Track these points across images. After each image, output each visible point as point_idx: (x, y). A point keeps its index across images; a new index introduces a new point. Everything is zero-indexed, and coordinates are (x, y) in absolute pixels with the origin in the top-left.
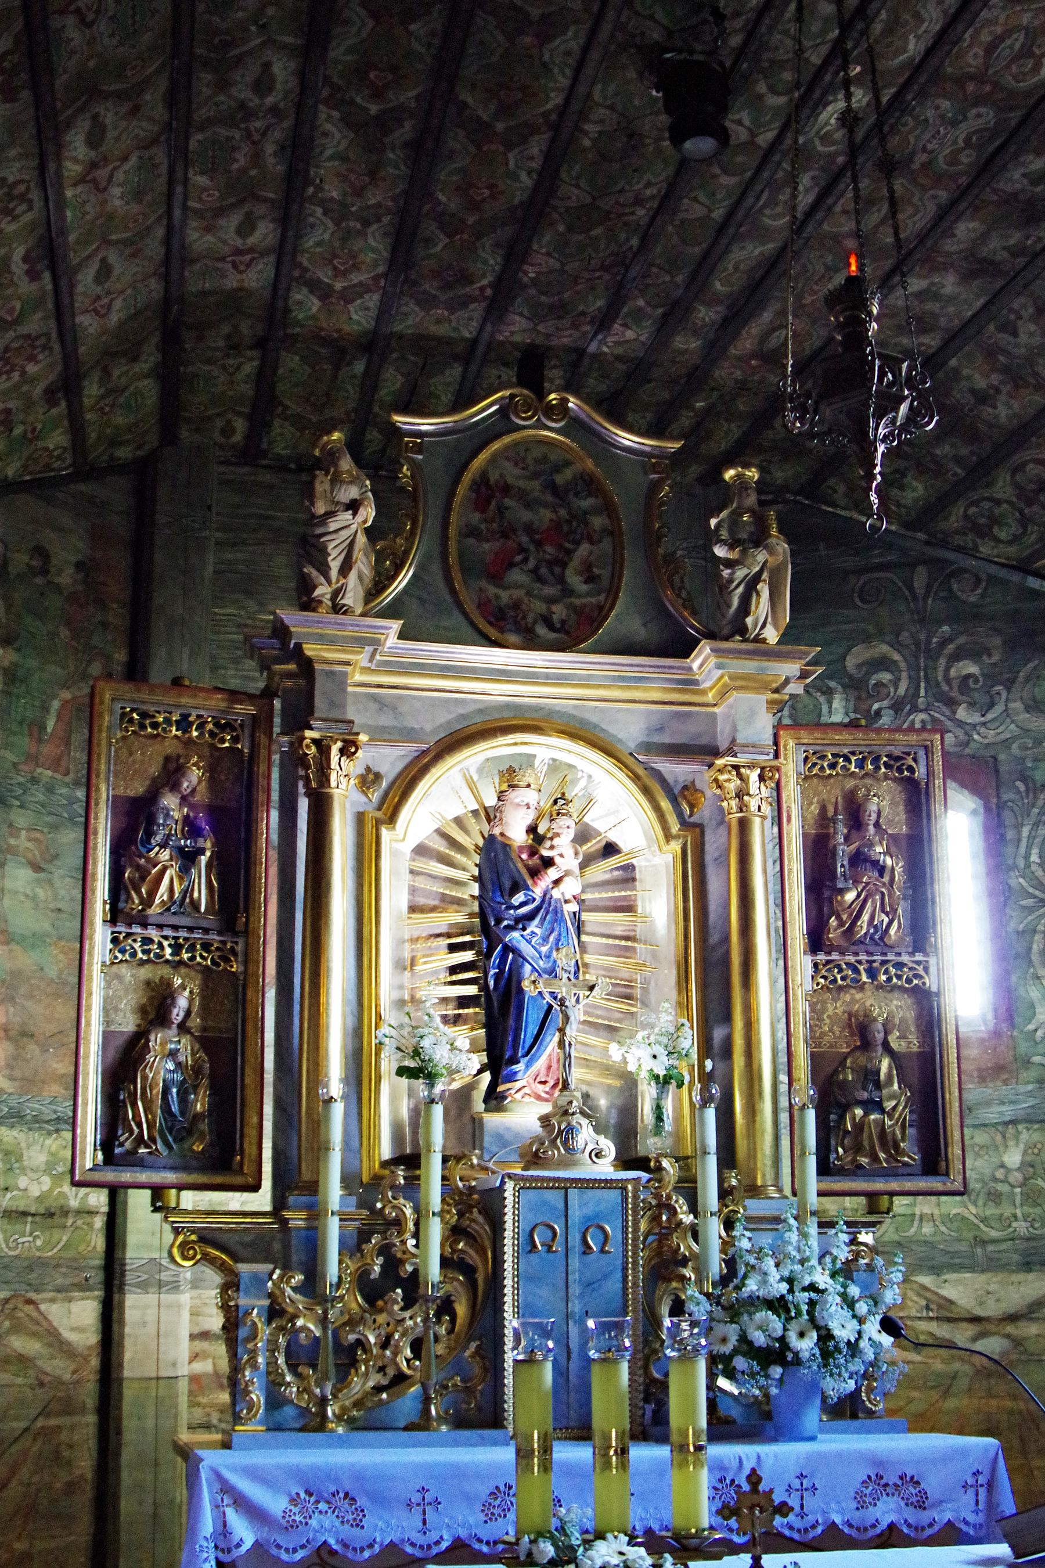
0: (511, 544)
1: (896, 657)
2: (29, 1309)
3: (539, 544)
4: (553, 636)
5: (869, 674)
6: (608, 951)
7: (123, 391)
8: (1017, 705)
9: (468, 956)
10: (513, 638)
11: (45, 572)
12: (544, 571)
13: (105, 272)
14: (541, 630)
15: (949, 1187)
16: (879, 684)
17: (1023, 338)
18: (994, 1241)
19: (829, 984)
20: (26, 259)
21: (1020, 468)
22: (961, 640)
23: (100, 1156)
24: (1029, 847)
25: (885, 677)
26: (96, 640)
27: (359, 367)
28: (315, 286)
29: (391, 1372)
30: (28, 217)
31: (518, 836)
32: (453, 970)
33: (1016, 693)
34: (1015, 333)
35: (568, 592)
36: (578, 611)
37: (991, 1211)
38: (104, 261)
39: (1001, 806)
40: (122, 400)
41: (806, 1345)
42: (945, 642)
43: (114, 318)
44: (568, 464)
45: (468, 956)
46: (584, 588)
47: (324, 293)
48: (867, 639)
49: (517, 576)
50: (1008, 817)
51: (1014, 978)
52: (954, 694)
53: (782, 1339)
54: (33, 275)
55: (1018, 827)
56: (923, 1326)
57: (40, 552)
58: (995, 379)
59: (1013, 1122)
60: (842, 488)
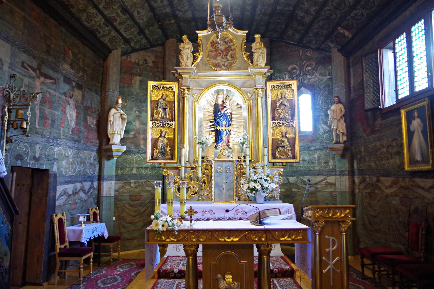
0: (218, 52)
1: (297, 67)
2: (149, 183)
3: (222, 52)
4: (225, 68)
5: (292, 70)
6: (237, 122)
7: (154, 32)
8: (318, 74)
9: (213, 123)
10: (218, 69)
11: (146, 63)
12: (223, 57)
13: (139, 13)
14: (223, 67)
15: (296, 161)
16: (294, 72)
17: (306, 5)
18: (313, 171)
19: (276, 126)
20: (121, 12)
21: (312, 30)
22: (308, 63)
23: (151, 158)
24: (319, 100)
25: (295, 71)
26: (157, 74)
27: (194, 23)
28: (179, 10)
29: (195, 192)
30: (118, 5)
31: (220, 102)
32: (211, 126)
33: (318, 72)
34: (304, 5)
35: (228, 60)
36: (230, 63)
37: (312, 165)
38: (137, 11)
39: (315, 93)
40: (154, 33)
41: (259, 188)
42: (305, 64)
43: (145, 20)
44: (227, 37)
45: (213, 123)
46: (231, 59)
47: (182, 12)
48: (292, 64)
49: (219, 58)
50: (316, 95)
51: (316, 124)
52: (307, 73)
53: (254, 187)
54: (125, 15)
55: (318, 97)
56: (301, 185)
57: (145, 60)
58: (303, 14)
59: (316, 150)
60: (286, 37)
